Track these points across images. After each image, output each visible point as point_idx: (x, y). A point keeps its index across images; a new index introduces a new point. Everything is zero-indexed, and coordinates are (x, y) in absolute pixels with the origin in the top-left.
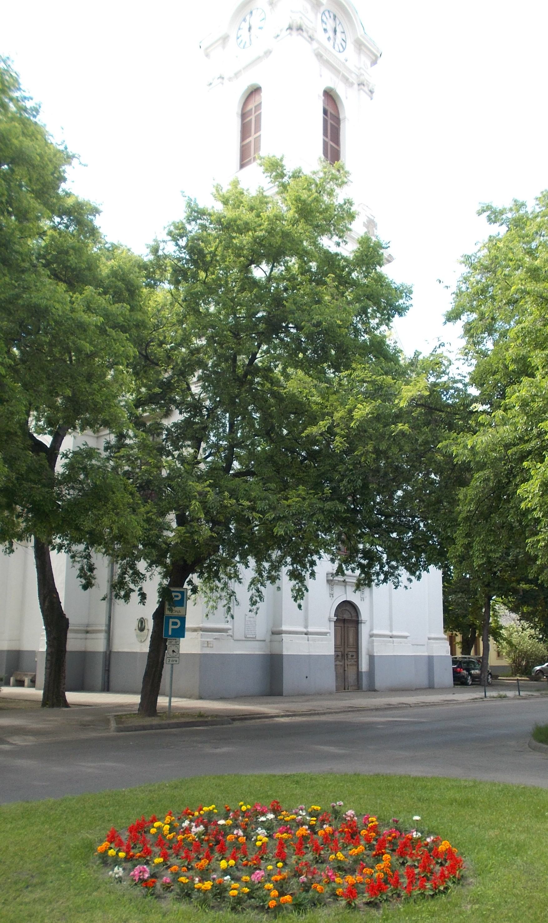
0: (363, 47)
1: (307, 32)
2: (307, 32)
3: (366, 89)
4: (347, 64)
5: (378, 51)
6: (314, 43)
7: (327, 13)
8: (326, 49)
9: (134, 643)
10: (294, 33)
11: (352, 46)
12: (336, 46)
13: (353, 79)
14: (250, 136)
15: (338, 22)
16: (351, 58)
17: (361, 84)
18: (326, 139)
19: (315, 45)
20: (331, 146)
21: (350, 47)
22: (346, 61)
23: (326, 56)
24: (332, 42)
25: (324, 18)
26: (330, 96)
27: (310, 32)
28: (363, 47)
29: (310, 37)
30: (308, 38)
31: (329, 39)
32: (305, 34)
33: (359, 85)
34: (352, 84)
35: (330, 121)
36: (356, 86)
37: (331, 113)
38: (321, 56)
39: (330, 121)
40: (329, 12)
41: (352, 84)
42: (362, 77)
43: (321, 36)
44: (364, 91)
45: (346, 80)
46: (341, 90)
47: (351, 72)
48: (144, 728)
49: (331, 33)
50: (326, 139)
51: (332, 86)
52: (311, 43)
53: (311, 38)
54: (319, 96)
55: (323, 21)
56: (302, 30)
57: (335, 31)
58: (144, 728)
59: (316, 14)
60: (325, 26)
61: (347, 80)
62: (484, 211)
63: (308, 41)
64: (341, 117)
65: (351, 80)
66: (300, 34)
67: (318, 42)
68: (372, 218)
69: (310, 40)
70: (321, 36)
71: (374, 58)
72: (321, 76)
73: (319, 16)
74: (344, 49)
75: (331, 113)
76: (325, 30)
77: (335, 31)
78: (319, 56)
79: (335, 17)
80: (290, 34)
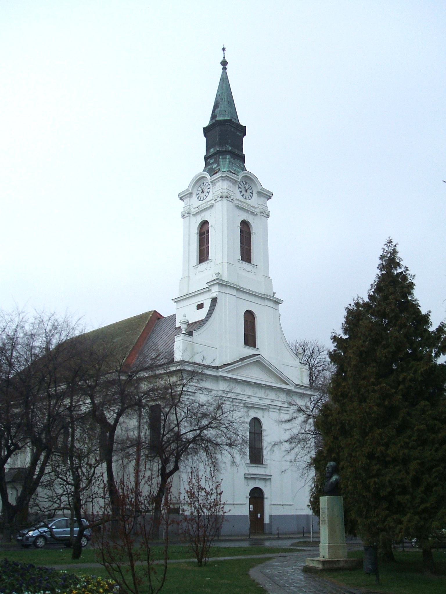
10: (224, 199)
13: (257, 211)
14: (204, 245)
21: (255, 195)
46: (250, 219)
78: (237, 206)
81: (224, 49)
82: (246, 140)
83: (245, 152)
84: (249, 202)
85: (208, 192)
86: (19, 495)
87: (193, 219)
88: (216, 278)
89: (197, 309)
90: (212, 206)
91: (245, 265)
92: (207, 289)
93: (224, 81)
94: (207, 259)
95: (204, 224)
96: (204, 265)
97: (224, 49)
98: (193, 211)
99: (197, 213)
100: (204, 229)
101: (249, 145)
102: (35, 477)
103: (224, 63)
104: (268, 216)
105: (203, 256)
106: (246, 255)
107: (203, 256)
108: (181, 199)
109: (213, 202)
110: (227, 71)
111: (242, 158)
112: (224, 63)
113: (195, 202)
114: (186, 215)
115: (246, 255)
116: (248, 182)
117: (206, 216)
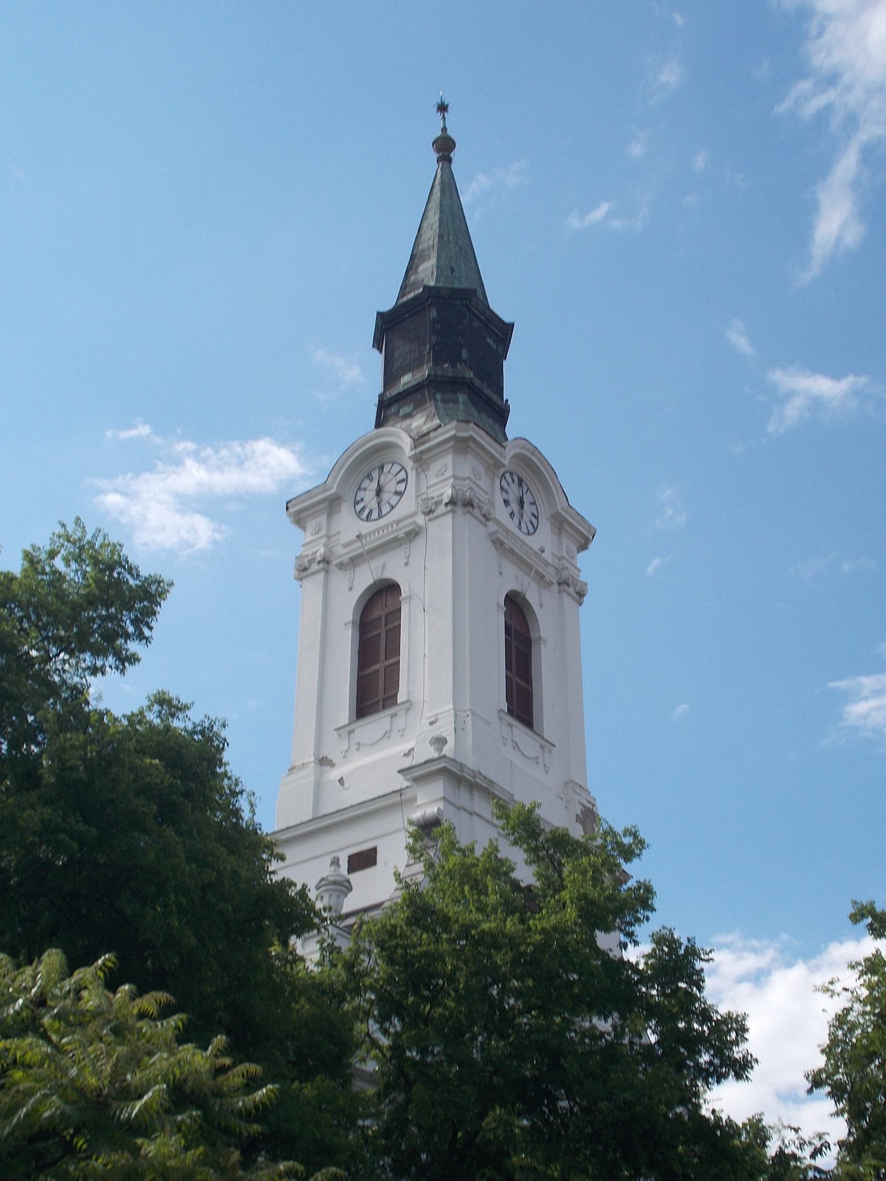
0: (565, 526)
1: (480, 509)
2: (480, 509)
3: (571, 590)
4: (543, 555)
5: (589, 531)
6: (490, 524)
7: (508, 476)
8: (508, 532)
9: (431, 483)
10: (460, 510)
11: (548, 524)
12: (523, 525)
13: (550, 575)
14: (377, 661)
15: (525, 489)
16: (543, 540)
17: (563, 583)
18: (508, 638)
19: (492, 527)
20: (518, 684)
21: (545, 526)
22: (543, 551)
23: (508, 544)
24: (516, 520)
25: (504, 483)
26: (516, 608)
27: (485, 508)
28: (565, 526)
29: (484, 516)
30: (481, 518)
31: (512, 515)
32: (476, 512)
33: (559, 584)
34: (550, 584)
35: (514, 644)
36: (555, 587)
37: (515, 630)
38: (502, 544)
39: (514, 644)
40: (511, 474)
41: (550, 584)
42: (565, 574)
43: (501, 513)
44: (569, 594)
45: (540, 578)
46: (532, 595)
47: (547, 564)
48: (440, 482)
49: (515, 507)
50: (510, 675)
51: (516, 587)
52: (485, 525)
53: (486, 517)
54: (498, 605)
55: (502, 488)
56: (473, 506)
57: (521, 503)
58: (440, 482)
59: (493, 480)
60: (506, 496)
61: (542, 577)
62: (863, 916)
63: (481, 522)
64: (533, 636)
65: (548, 578)
66: (469, 512)
67: (498, 523)
68: (591, 807)
69: (484, 520)
70: (501, 513)
71: (583, 541)
72: (501, 574)
73: (497, 481)
74: (535, 529)
75: (515, 630)
76: (506, 502)
77: (521, 503)
78: (498, 543)
79: (520, 481)
80: (453, 511)
81: (443, 108)
82: (513, 368)
83: (508, 393)
84: (528, 539)
85: (400, 494)
86: (172, 1163)
87: (340, 580)
88: (436, 755)
89: (376, 848)
90: (413, 534)
91: (519, 731)
92: (397, 799)
93: (448, 190)
94: (390, 700)
95: (385, 592)
96: (377, 724)
97: (443, 108)
98: (341, 553)
99: (355, 561)
100: (378, 612)
101: (520, 377)
102: (574, 223)
103: (445, 147)
104: (581, 595)
105: (374, 689)
106: (521, 704)
107: (374, 689)
108: (299, 520)
109: (421, 520)
110: (454, 167)
111: (499, 413)
112: (445, 147)
113: (348, 526)
114: (315, 567)
115: (521, 704)
116: (529, 476)
117: (392, 567)
